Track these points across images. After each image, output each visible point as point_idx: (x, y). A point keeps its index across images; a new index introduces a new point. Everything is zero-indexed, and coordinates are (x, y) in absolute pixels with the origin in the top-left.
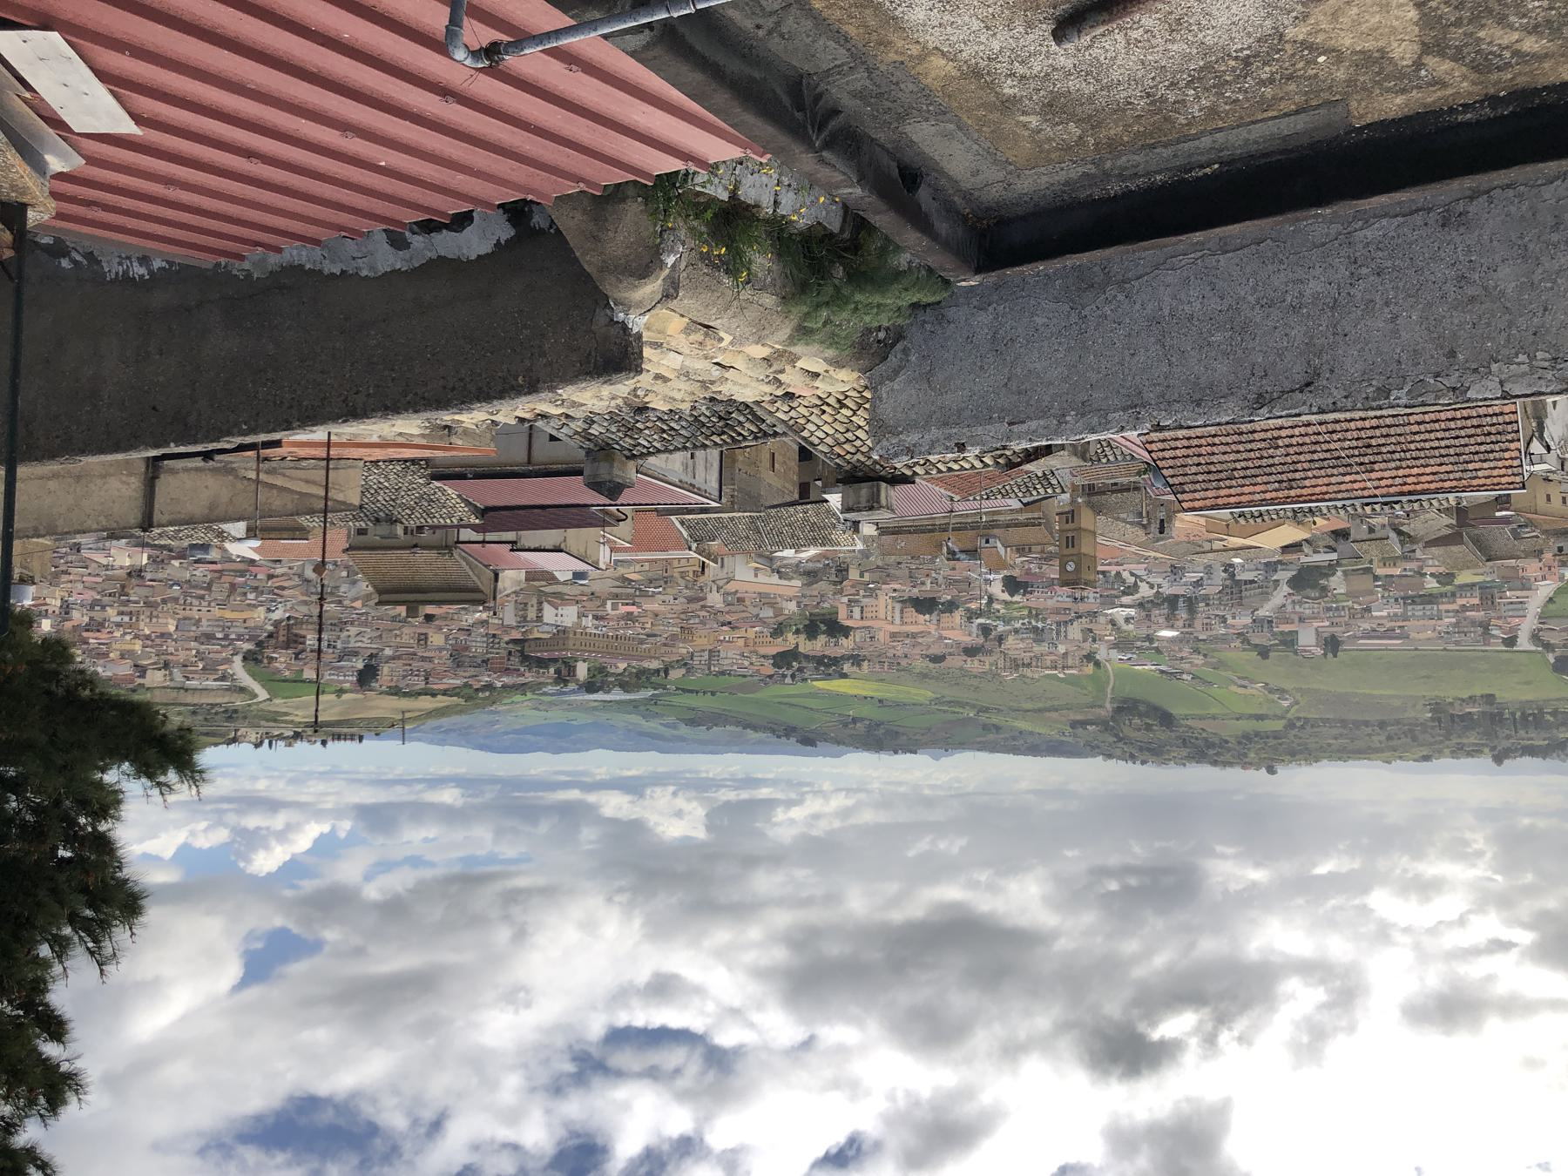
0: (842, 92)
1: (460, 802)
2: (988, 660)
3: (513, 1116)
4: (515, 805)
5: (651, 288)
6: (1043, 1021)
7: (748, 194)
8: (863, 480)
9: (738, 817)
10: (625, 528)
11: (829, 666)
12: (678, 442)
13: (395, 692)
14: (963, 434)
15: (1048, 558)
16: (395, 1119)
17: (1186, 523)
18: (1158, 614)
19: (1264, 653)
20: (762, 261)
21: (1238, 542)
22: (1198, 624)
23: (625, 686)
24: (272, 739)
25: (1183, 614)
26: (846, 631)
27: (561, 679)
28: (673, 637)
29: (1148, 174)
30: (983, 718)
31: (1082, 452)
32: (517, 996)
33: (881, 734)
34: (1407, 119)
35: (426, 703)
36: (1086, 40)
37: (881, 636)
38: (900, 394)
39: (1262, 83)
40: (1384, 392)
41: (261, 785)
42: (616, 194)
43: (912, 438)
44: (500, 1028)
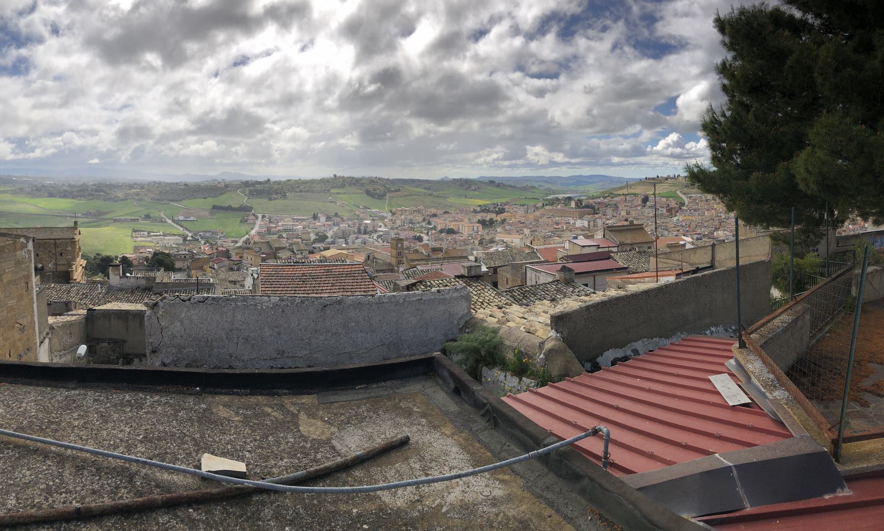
0: (480, 423)
1: (612, 157)
2: (429, 213)
3: (589, 49)
4: (593, 157)
5: (548, 346)
6: (415, 85)
7: (515, 380)
8: (473, 277)
9: (516, 155)
10: (560, 255)
11: (485, 210)
12: (541, 287)
13: (635, 195)
14: (438, 296)
15: (408, 248)
16: (627, 49)
17: (361, 258)
18: (370, 229)
19: (336, 215)
20: (510, 356)
21: (344, 252)
22: (357, 224)
23: (558, 199)
24: (674, 178)
25: (362, 228)
26: (479, 222)
27: (580, 201)
28: (541, 218)
29: (378, 387)
30: (430, 192)
31: (396, 288)
32: (589, 91)
33: (466, 185)
34: (301, 394)
35: (625, 191)
36: (399, 436)
37: (467, 220)
38: (460, 309)
39: (344, 414)
40: (302, 302)
41: (677, 163)
42: (561, 378)
43: (455, 295)
44: (595, 79)
